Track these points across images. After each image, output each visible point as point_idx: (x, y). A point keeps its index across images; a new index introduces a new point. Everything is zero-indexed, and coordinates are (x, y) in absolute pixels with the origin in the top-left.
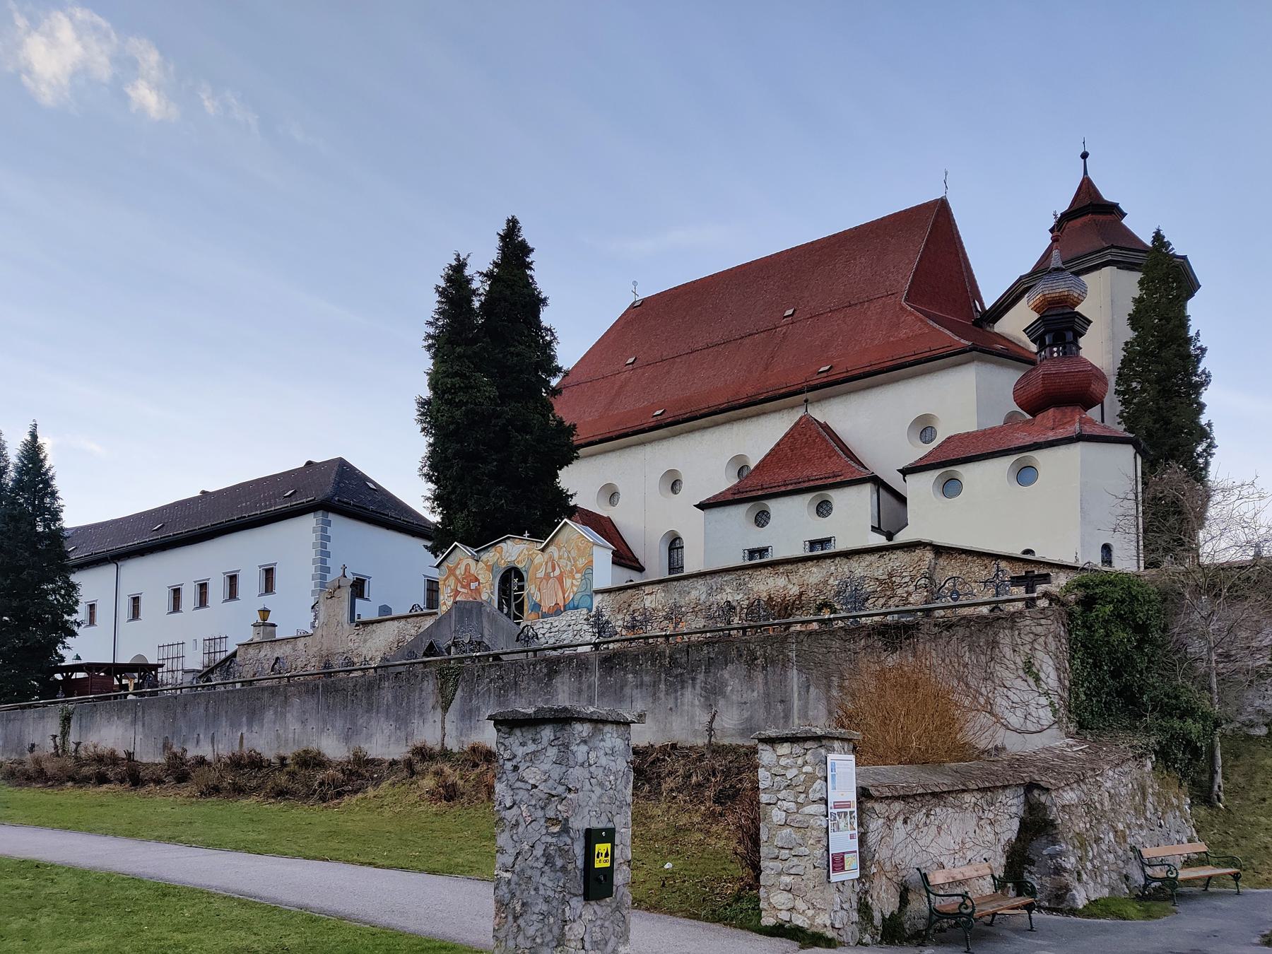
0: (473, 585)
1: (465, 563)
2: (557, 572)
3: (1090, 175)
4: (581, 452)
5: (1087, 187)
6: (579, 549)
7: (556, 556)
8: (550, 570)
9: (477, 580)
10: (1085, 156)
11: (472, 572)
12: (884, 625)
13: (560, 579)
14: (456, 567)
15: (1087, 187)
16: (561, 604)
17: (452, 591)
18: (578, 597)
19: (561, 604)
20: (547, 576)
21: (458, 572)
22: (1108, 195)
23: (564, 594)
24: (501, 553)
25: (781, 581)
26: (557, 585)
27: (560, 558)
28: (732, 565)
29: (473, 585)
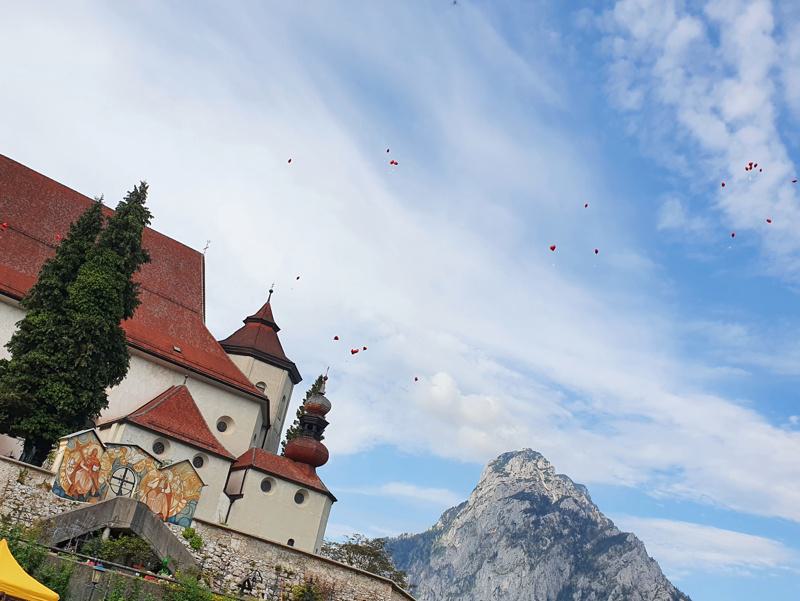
0: (95, 468)
1: (94, 447)
2: (168, 491)
3: (271, 302)
4: (264, 432)
5: (267, 309)
6: (190, 483)
7: (170, 478)
8: (162, 486)
9: (99, 465)
10: (271, 291)
11: (98, 457)
12: (605, 413)
13: (169, 496)
14: (85, 447)
15: (267, 309)
16: (165, 515)
17: (75, 463)
18: (179, 516)
19: (165, 515)
20: (158, 490)
21: (85, 451)
22: (277, 320)
23: (169, 509)
24: (125, 454)
25: (323, 571)
26: (165, 500)
27: (173, 481)
28: (277, 541)
29: (95, 468)
